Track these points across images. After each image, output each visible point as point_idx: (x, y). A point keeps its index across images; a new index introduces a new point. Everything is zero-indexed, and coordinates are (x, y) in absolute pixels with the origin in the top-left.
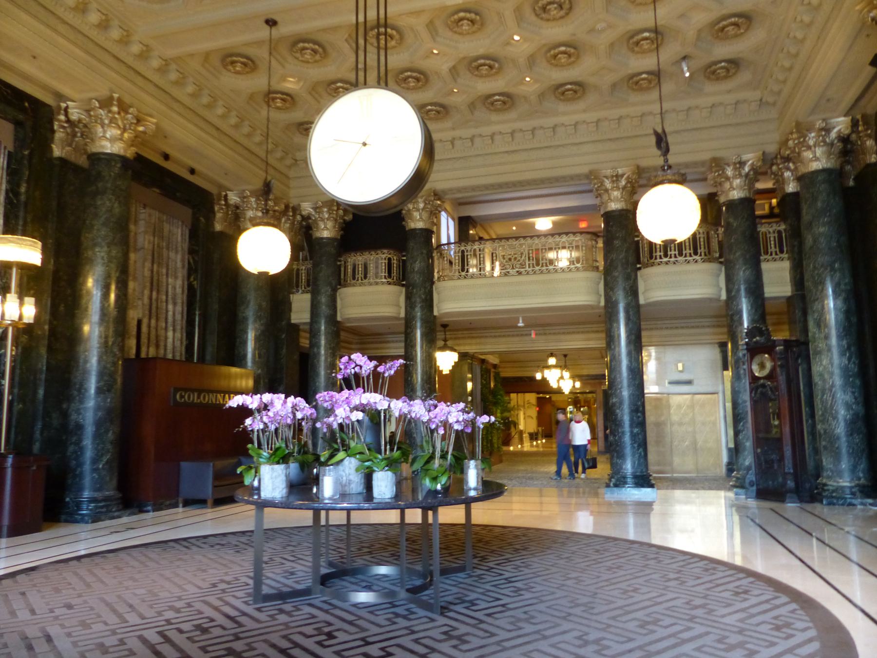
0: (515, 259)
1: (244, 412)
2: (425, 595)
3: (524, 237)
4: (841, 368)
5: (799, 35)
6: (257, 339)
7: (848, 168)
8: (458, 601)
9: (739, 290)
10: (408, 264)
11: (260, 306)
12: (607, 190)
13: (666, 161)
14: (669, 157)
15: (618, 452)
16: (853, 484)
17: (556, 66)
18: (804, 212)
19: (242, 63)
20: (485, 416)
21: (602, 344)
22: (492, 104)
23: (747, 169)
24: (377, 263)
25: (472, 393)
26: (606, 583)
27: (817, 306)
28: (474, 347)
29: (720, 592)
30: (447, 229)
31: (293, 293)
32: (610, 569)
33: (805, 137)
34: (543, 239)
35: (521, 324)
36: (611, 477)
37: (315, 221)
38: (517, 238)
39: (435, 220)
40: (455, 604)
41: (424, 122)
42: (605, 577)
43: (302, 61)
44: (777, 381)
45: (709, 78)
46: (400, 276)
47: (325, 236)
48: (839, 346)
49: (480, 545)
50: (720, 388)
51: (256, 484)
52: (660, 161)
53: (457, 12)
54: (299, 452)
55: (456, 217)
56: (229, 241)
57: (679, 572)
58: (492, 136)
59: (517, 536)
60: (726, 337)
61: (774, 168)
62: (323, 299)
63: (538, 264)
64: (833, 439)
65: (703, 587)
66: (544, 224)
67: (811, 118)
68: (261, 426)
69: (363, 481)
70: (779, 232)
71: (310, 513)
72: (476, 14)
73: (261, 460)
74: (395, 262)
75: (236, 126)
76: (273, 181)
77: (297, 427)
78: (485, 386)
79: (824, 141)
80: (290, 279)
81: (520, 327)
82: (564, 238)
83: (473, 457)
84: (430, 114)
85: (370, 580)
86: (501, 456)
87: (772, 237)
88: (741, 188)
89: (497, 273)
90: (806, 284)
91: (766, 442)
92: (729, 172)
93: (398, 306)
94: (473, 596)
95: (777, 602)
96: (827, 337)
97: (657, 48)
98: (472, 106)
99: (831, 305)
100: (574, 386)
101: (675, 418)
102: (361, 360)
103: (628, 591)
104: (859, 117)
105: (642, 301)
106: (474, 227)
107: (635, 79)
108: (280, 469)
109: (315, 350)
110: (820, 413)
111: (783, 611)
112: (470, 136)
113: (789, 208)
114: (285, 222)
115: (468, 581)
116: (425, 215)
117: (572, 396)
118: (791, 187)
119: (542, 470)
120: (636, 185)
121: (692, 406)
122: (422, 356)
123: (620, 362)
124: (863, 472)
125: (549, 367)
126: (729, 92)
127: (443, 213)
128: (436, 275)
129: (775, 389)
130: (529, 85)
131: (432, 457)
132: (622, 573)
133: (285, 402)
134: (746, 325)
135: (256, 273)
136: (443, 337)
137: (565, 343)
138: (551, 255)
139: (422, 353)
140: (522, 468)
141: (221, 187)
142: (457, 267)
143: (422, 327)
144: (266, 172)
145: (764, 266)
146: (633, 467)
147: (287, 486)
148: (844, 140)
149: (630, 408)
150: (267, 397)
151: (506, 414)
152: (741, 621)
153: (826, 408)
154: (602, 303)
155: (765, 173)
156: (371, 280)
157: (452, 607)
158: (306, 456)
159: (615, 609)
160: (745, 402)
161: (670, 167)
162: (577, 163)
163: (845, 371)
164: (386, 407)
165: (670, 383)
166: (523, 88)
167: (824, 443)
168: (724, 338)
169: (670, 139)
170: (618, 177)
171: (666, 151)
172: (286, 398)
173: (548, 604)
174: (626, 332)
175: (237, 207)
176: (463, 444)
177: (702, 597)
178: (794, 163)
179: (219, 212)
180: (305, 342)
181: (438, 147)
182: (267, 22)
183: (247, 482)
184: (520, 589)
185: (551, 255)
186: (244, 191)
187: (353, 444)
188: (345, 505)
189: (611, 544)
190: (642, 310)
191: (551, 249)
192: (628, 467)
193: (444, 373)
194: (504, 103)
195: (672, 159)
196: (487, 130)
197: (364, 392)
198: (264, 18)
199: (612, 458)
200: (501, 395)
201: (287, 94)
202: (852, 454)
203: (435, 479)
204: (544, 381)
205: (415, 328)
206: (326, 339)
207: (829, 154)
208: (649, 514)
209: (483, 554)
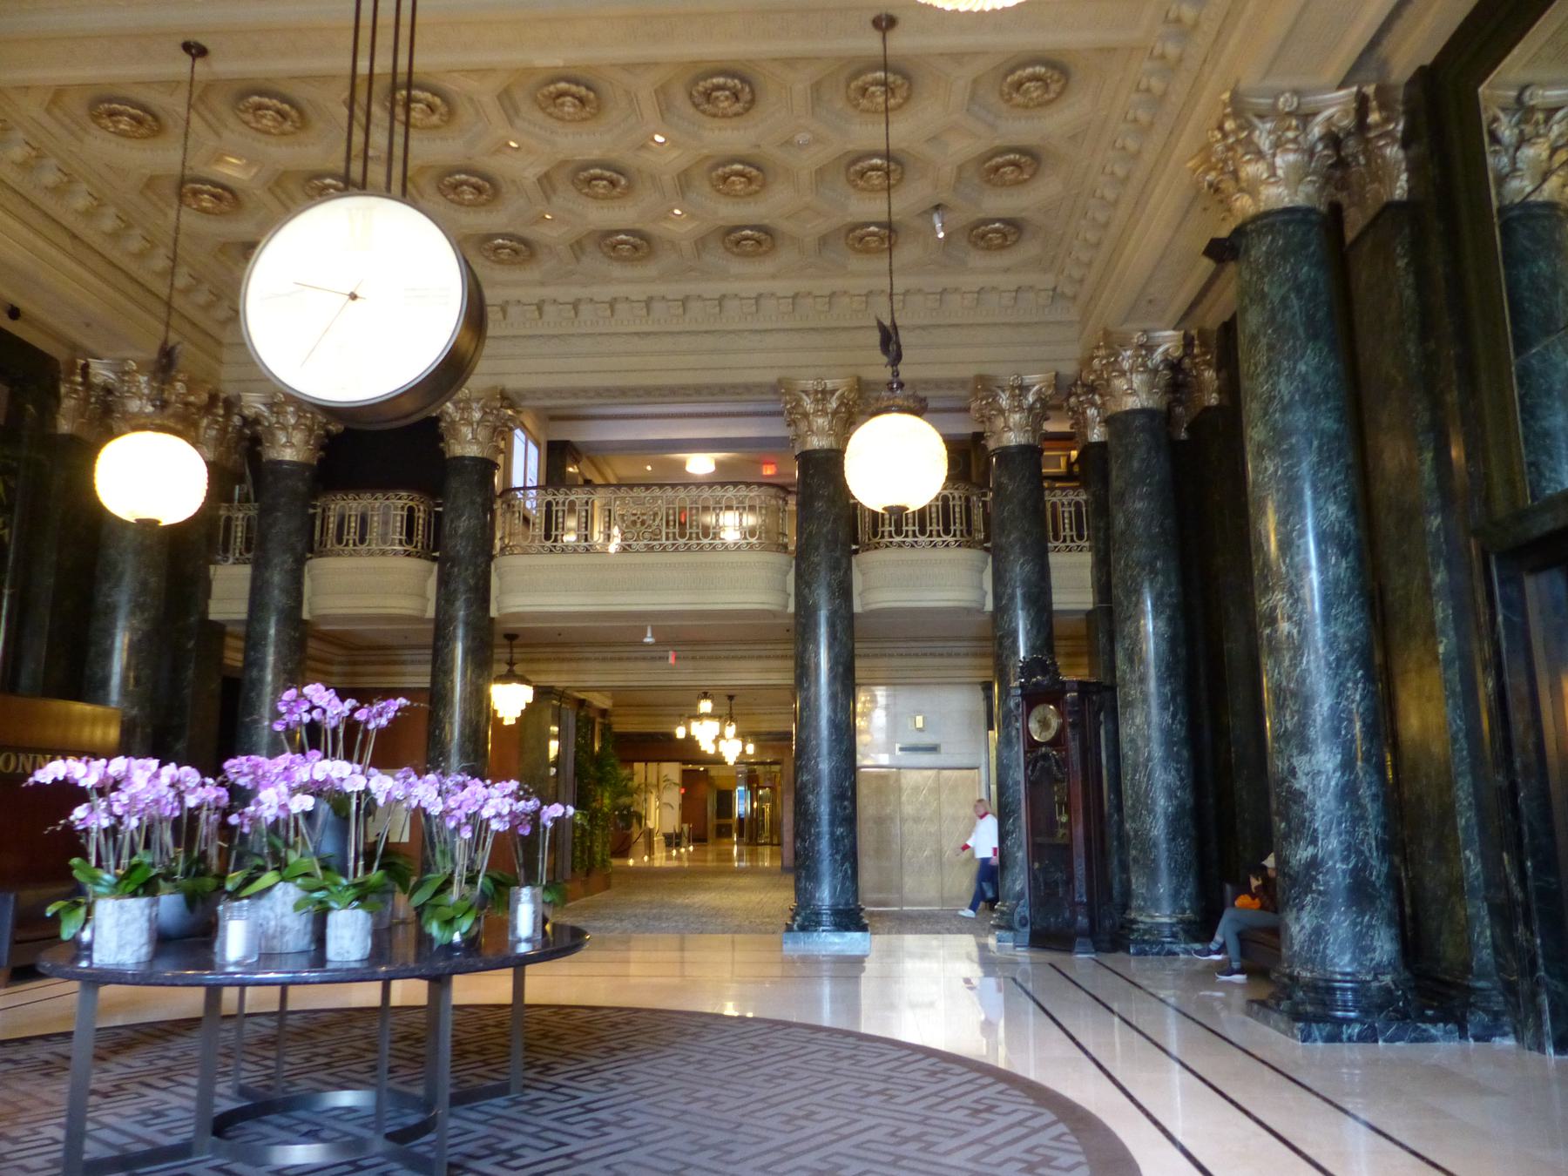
0: (643, 523)
1: (70, 793)
2: (421, 1146)
3: (661, 486)
4: (1161, 730)
5: (1110, 194)
6: (133, 649)
7: (1179, 410)
8: (486, 1152)
9: (1012, 597)
10: (447, 521)
11: (144, 584)
12: (806, 415)
13: (896, 374)
14: (900, 367)
15: (808, 869)
16: (1174, 920)
17: (727, 194)
18: (1114, 473)
19: (132, 117)
20: (557, 805)
21: (788, 679)
22: (614, 247)
23: (1031, 399)
24: (386, 514)
25: (558, 762)
26: (760, 1105)
27: (1129, 628)
28: (564, 677)
29: (950, 1111)
30: (524, 463)
31: (216, 563)
32: (771, 1078)
33: (1117, 355)
34: (694, 492)
35: (649, 640)
36: (795, 913)
37: (270, 430)
38: (648, 486)
39: (502, 444)
40: (479, 1158)
41: (466, 262)
42: (761, 1094)
43: (257, 130)
44: (1066, 750)
45: (975, 245)
46: (430, 541)
47: (288, 458)
48: (1160, 694)
49: (545, 1042)
50: (983, 760)
51: (86, 936)
52: (886, 374)
53: (554, 81)
54: (186, 873)
55: (543, 440)
56: (83, 452)
57: (887, 1079)
58: (612, 304)
59: (614, 1025)
60: (990, 673)
61: (1073, 400)
62: (277, 578)
63: (682, 535)
64: (1147, 845)
65: (923, 1104)
66: (700, 464)
67: (1125, 327)
68: (105, 823)
69: (310, 927)
70: (1078, 504)
71: (200, 992)
72: (589, 88)
73: (98, 889)
74: (421, 516)
75: (115, 236)
76: (179, 348)
77: (186, 826)
78: (583, 748)
79: (1144, 365)
80: (210, 539)
81: (648, 644)
82: (731, 492)
83: (531, 880)
84: (476, 253)
85: (320, 1119)
86: (608, 876)
87: (1066, 513)
88: (1020, 428)
89: (613, 547)
90: (1114, 592)
91: (1048, 851)
92: (1004, 400)
93: (423, 596)
94: (515, 1140)
95: (1036, 1123)
96: (1143, 680)
97: (889, 188)
98: (578, 247)
99: (1150, 628)
100: (744, 752)
101: (909, 809)
102: (321, 698)
103: (796, 1118)
104: (1194, 332)
105: (857, 608)
106: (576, 461)
107: (859, 233)
108: (137, 907)
109: (255, 673)
110: (1130, 803)
111: (1043, 1138)
112: (571, 299)
113: (1093, 466)
114: (208, 427)
115: (513, 1112)
116: (482, 434)
117: (743, 768)
118: (1096, 434)
119: (679, 901)
120: (856, 410)
121: (937, 790)
122: (462, 691)
123: (818, 711)
124: (1189, 900)
125: (700, 717)
126: (1007, 270)
127: (518, 432)
128: (498, 543)
129: (1063, 763)
130: (679, 222)
131: (448, 883)
132: (790, 1085)
133: (156, 776)
134: (1022, 654)
135: (132, 520)
136: (508, 656)
137: (728, 676)
138: (709, 519)
139: (464, 685)
140: (645, 898)
141: (75, 348)
142: (539, 531)
143: (466, 636)
144: (168, 325)
145: (1053, 558)
146: (833, 895)
147: (150, 941)
148: (1174, 366)
149: (831, 791)
150: (119, 765)
151: (624, 800)
152: (975, 1159)
153: (1137, 793)
154: (791, 609)
155: (1058, 408)
156: (374, 546)
157: (473, 1164)
158: (201, 880)
159: (768, 1152)
160: (1017, 783)
161: (901, 385)
162: (758, 363)
163: (1167, 733)
164: (362, 788)
165: (901, 749)
166: (670, 226)
167: (1134, 853)
168: (988, 674)
169: (905, 338)
170: (825, 394)
171: (896, 359)
172: (161, 766)
173: (651, 1148)
174: (830, 659)
175: (108, 390)
176: (514, 857)
177: (919, 1123)
178: (1101, 396)
179: (67, 395)
180: (234, 657)
181: (493, 315)
182: (187, 47)
183: (67, 933)
184: (605, 1123)
185: (709, 519)
186: (125, 360)
187: (293, 857)
188: (272, 975)
189: (779, 1034)
190: (857, 623)
191: (706, 509)
192: (825, 895)
193: (506, 723)
194: (635, 248)
195: (906, 373)
196: (604, 292)
197: (326, 757)
198: (181, 40)
199: (798, 880)
200: (613, 766)
201: (224, 188)
202: (1177, 871)
203: (449, 923)
204: (690, 740)
205: (453, 639)
206: (278, 653)
207: (1151, 386)
208: (857, 978)
209: (547, 1060)
